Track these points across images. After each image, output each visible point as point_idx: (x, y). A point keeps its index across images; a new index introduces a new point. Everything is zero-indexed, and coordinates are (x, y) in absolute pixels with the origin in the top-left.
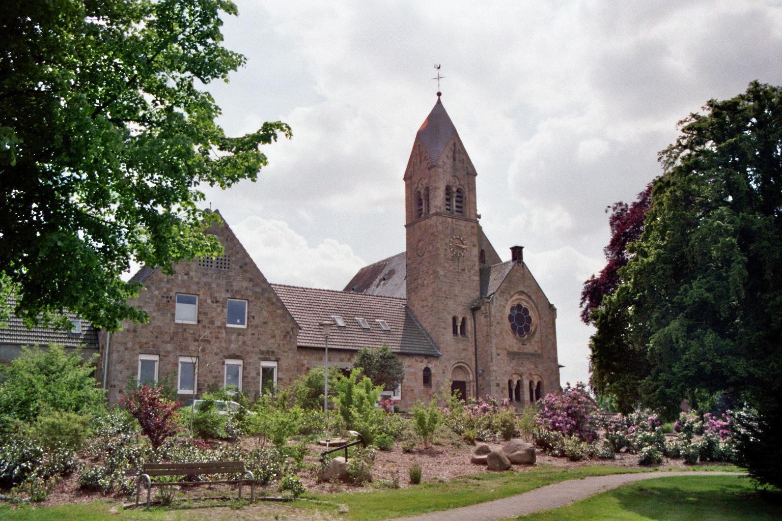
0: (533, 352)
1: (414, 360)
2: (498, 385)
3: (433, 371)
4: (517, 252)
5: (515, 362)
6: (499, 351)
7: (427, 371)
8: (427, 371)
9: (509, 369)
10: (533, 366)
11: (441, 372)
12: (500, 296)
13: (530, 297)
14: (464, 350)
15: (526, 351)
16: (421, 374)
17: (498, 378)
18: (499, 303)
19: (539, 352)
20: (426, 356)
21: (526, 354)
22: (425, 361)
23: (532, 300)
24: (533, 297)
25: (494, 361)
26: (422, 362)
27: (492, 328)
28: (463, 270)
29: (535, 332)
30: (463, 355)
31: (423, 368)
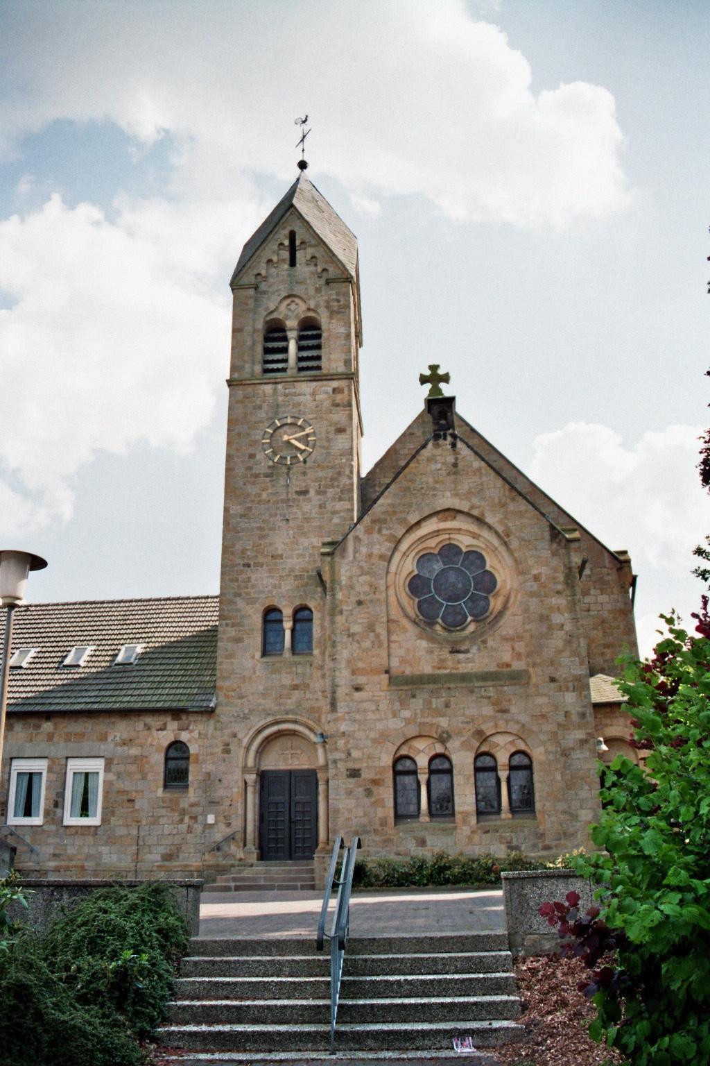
0: (493, 668)
1: (140, 726)
2: (354, 773)
3: (193, 749)
4: (701, 452)
5: (418, 703)
6: (361, 680)
7: (177, 751)
8: (177, 751)
9: (395, 724)
10: (488, 710)
11: (219, 750)
12: (368, 531)
13: (480, 521)
14: (296, 687)
15: (464, 668)
16: (158, 759)
17: (355, 754)
18: (364, 550)
19: (517, 665)
20: (176, 713)
21: (464, 678)
22: (173, 725)
23: (490, 527)
24: (489, 519)
25: (342, 707)
26: (163, 728)
27: (340, 619)
28: (304, 492)
29: (501, 614)
30: (290, 703)
31: (165, 744)
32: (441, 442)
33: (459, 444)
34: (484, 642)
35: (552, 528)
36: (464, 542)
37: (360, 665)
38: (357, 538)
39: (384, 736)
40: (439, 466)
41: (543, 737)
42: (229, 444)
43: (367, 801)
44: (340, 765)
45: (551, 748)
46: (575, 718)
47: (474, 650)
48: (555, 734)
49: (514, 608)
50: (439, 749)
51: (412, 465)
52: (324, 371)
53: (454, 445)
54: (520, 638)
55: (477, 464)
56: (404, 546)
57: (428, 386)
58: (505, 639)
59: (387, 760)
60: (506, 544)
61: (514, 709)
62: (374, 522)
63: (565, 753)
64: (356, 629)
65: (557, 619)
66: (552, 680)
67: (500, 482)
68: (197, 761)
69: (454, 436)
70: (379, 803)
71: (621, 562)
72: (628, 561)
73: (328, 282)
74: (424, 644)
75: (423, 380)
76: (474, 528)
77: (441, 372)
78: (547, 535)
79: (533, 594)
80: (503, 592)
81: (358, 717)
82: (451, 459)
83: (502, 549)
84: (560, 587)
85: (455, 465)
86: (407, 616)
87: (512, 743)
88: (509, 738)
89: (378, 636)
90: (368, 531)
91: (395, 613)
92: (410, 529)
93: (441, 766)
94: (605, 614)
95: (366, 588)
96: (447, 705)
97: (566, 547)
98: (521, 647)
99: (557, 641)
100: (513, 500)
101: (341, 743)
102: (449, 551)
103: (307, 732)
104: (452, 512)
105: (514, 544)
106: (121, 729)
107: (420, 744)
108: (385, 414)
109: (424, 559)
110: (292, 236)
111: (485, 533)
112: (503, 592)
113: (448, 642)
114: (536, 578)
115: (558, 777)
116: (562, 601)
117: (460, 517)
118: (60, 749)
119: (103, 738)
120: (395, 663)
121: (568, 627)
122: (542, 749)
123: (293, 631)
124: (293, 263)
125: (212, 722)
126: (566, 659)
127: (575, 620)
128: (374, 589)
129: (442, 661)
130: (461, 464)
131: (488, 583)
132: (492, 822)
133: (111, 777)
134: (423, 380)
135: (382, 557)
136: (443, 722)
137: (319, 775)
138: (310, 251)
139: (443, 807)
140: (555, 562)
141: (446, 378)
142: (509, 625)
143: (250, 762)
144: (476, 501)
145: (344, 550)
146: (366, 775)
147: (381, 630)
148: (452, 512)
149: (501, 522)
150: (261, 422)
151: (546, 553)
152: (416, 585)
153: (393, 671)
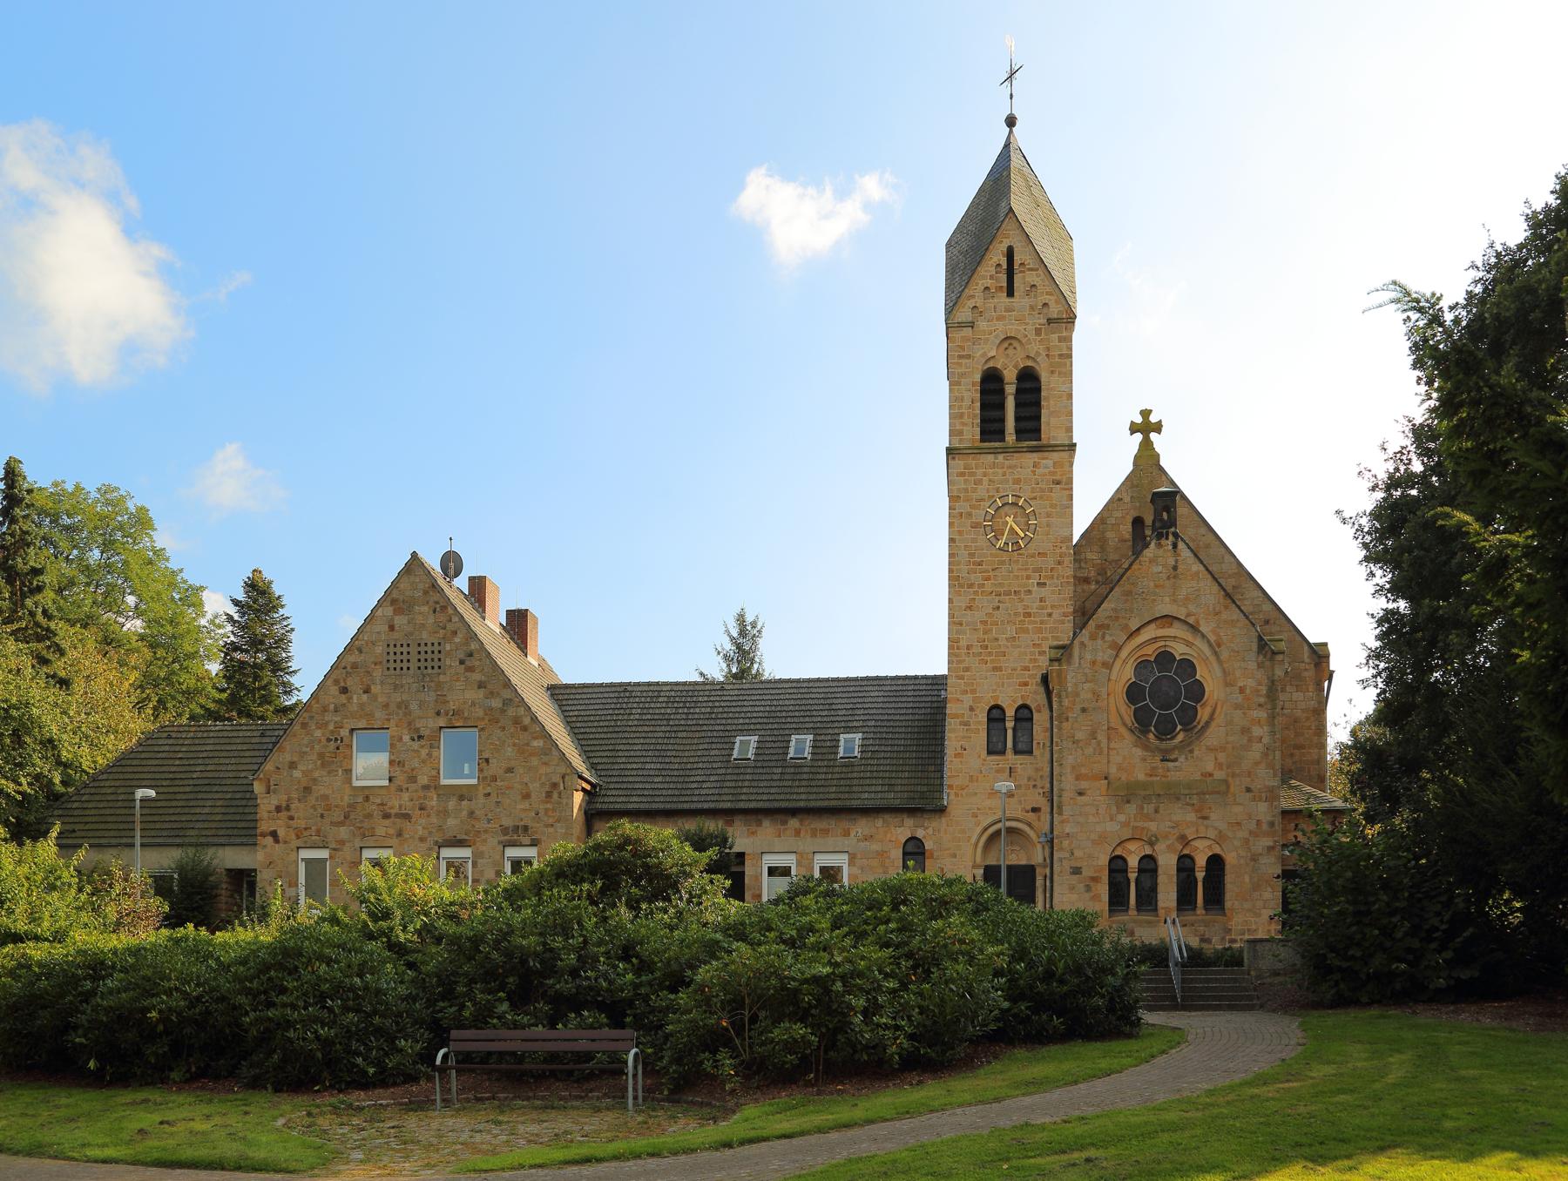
1: (879, 822)
2: (1076, 871)
3: (928, 845)
5: (1131, 809)
6: (1084, 785)
12: (1093, 637)
13: (1194, 628)
17: (1078, 853)
18: (1088, 657)
20: (912, 811)
23: (1203, 636)
29: (1207, 724)
32: (1163, 541)
33: (1181, 545)
34: (1191, 751)
35: (1260, 638)
36: (1179, 650)
37: (1083, 771)
38: (1082, 644)
39: (1103, 838)
40: (1160, 568)
41: (1237, 843)
42: (951, 524)
43: (1088, 895)
44: (1065, 863)
45: (1242, 853)
46: (1265, 827)
47: (1182, 759)
48: (1247, 841)
49: (1220, 719)
50: (1148, 851)
51: (1135, 567)
52: (1044, 442)
53: (1175, 546)
54: (1223, 749)
55: (1197, 567)
56: (1124, 653)
57: (1139, 437)
58: (1210, 749)
59: (1104, 860)
60: (1216, 653)
61: (1213, 816)
62: (1099, 627)
63: (1254, 859)
64: (1080, 735)
65: (1257, 731)
66: (1248, 790)
67: (1216, 587)
68: (932, 856)
69: (1176, 535)
70: (1096, 898)
71: (1320, 657)
72: (1328, 656)
73: (1050, 321)
74: (1138, 752)
75: (1134, 429)
76: (1189, 636)
77: (1153, 419)
78: (1255, 647)
79: (1237, 707)
80: (1211, 702)
81: (1081, 819)
82: (1171, 562)
83: (1212, 658)
84: (1262, 700)
85: (1175, 568)
86: (1125, 724)
87: (1210, 847)
88: (1208, 843)
89: (1099, 743)
90: (1093, 637)
91: (1115, 722)
92: (1131, 635)
93: (1149, 865)
94: (1299, 713)
95: (1090, 696)
96: (1156, 811)
97: (1272, 659)
98: (1222, 757)
99: (1256, 752)
100: (1226, 607)
101: (1066, 843)
102: (1165, 658)
103: (1026, 829)
104: (1168, 619)
105: (1225, 655)
106: (862, 827)
107: (1132, 846)
108: (1096, 481)
109: (1142, 666)
110: (1010, 254)
111: (1198, 642)
112: (1211, 702)
113: (1160, 750)
114: (1242, 690)
115: (1247, 879)
116: (1262, 714)
117: (1176, 624)
118: (806, 843)
119: (847, 834)
120: (1113, 770)
121: (1266, 740)
122: (1234, 854)
123: (1014, 730)
124: (1010, 293)
125: (943, 820)
126: (1262, 771)
127: (1273, 733)
128: (1097, 696)
129: (1153, 768)
130: (1181, 568)
131: (1197, 691)
132: (1189, 918)
133: (856, 871)
134: (1134, 429)
135: (1105, 664)
136: (1153, 826)
137: (1038, 870)
138: (1032, 278)
139: (1148, 900)
140: (1260, 675)
141: (1158, 428)
142: (1214, 736)
143: (978, 860)
144: (1192, 608)
145: (1070, 656)
146: (1086, 873)
147: (1102, 737)
148: (1168, 619)
149: (1213, 631)
150: (982, 500)
151: (1253, 665)
152: (1134, 693)
153: (1111, 777)
